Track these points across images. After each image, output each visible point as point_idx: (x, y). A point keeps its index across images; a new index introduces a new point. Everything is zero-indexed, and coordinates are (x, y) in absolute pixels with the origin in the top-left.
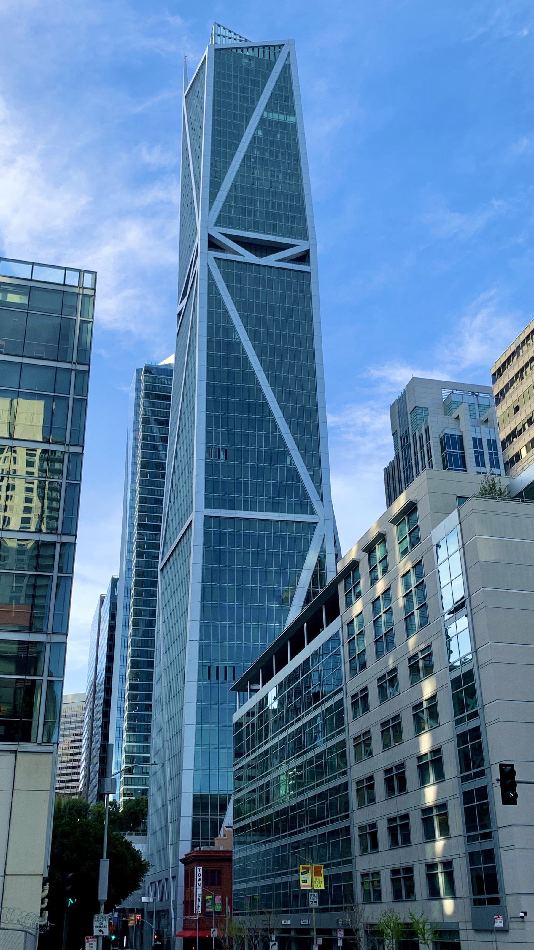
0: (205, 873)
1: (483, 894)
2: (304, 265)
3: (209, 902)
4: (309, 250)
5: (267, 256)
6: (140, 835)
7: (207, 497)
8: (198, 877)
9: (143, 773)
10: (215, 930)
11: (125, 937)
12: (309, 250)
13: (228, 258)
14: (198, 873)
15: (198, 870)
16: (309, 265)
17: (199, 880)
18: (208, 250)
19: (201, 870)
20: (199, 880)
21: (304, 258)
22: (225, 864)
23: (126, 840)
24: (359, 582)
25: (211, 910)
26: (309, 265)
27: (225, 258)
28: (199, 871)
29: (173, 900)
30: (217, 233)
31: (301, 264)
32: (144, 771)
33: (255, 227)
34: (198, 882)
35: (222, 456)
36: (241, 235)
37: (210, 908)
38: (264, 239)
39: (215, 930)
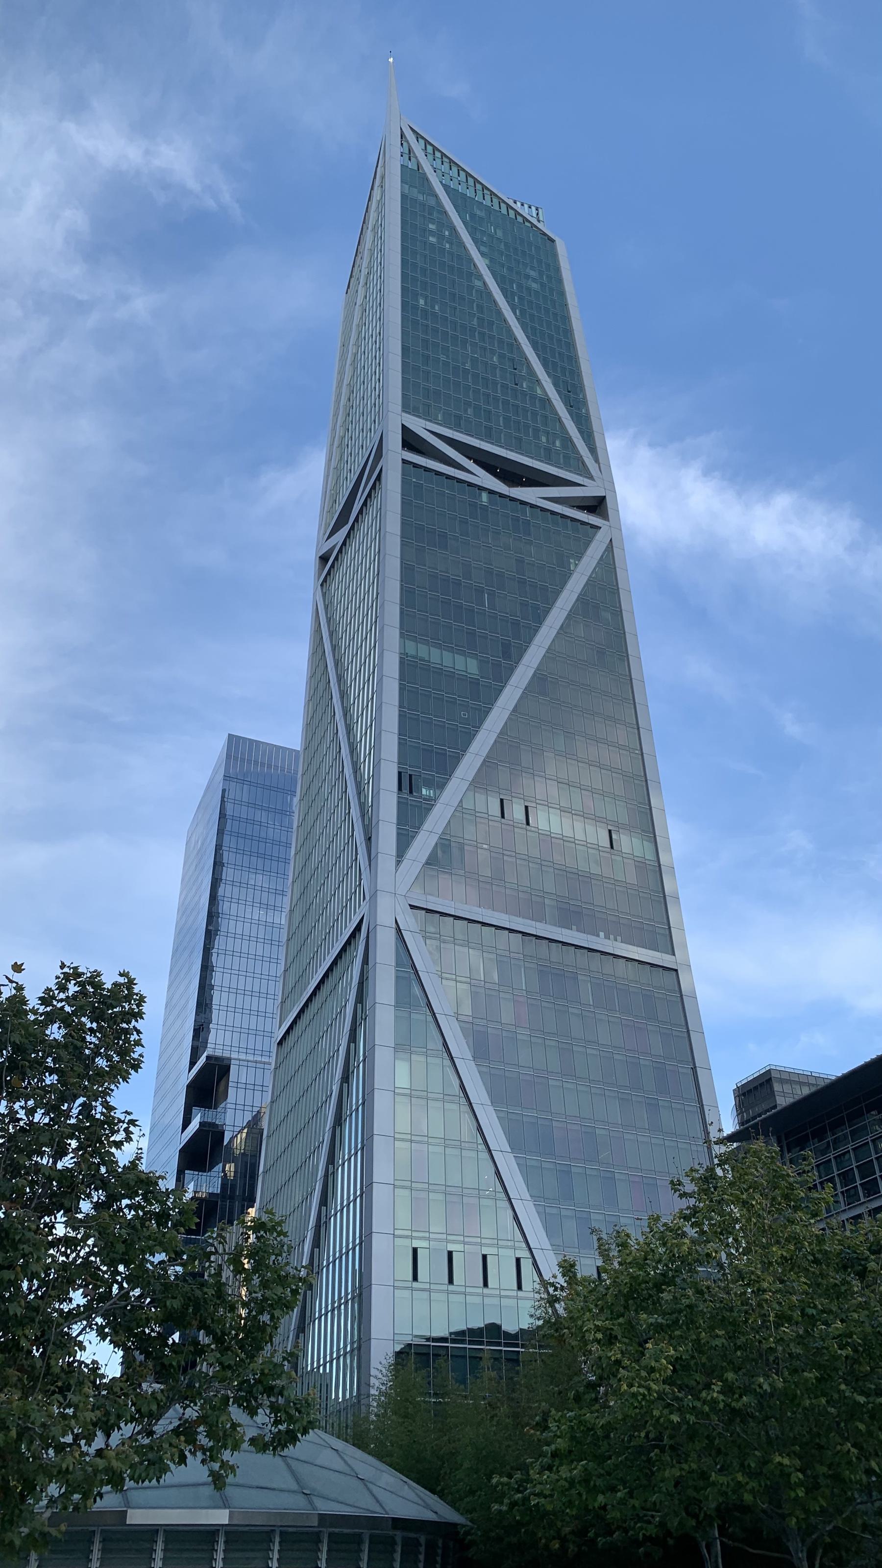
30: (418, 426)
33: (488, 436)
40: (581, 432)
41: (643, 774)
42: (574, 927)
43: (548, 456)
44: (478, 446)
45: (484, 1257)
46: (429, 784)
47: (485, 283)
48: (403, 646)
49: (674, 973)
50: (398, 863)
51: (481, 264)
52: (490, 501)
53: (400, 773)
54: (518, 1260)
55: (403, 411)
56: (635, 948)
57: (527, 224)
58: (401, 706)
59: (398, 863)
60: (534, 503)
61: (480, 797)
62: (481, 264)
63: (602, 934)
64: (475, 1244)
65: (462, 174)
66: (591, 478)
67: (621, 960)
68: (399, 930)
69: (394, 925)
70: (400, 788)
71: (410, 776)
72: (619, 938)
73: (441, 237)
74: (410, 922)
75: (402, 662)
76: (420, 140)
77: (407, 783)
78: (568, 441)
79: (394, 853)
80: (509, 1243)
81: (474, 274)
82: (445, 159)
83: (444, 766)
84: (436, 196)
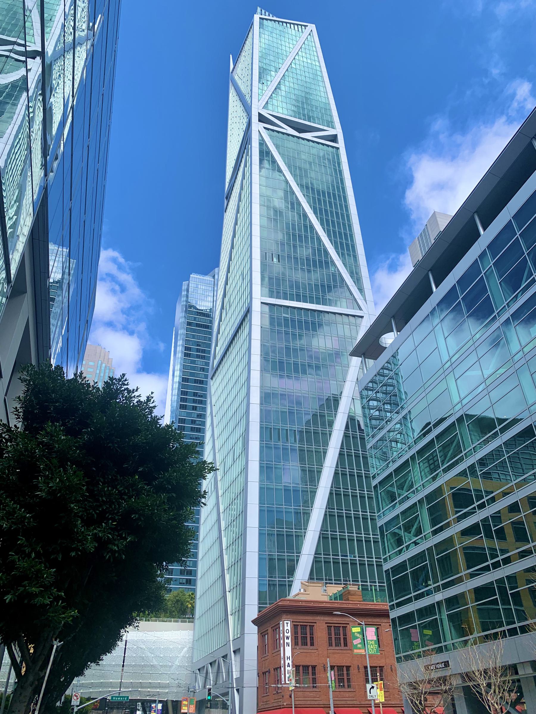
0: (295, 627)
3: (357, 638)
6: (186, 622)
8: (286, 634)
9: (180, 583)
10: (373, 687)
14: (286, 628)
15: (285, 625)
17: (288, 638)
19: (289, 625)
20: (288, 638)
22: (318, 618)
24: (358, 421)
25: (362, 652)
28: (286, 626)
29: (236, 679)
32: (181, 582)
34: (286, 641)
35: (275, 260)
37: (360, 649)
39: (373, 687)
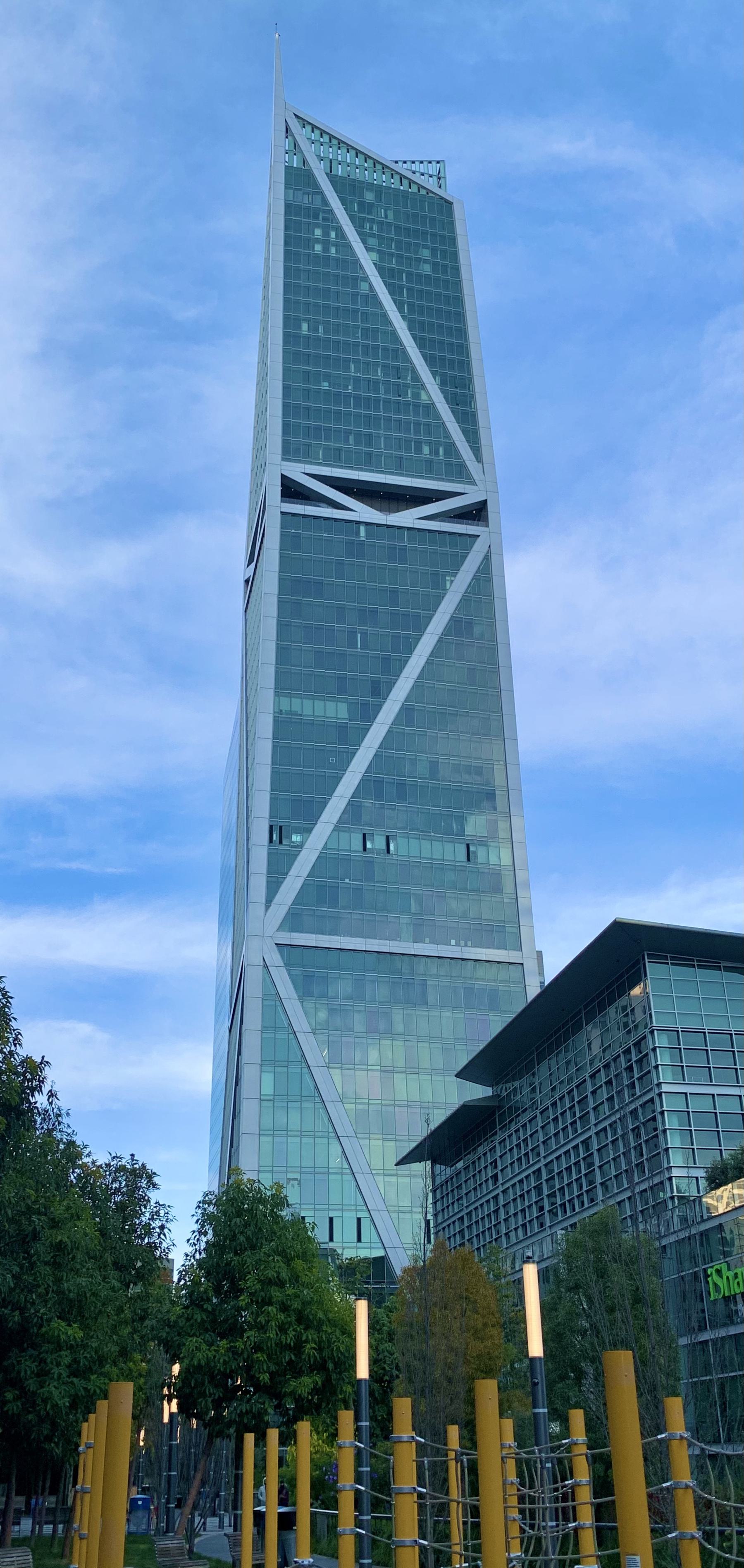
1: (525, 1504)
2: (478, 525)
4: (486, 501)
5: (398, 511)
7: (270, 879)
11: (536, 1348)
12: (486, 501)
13: (307, 513)
16: (487, 526)
18: (282, 501)
21: (477, 513)
23: (405, 1271)
26: (487, 526)
27: (302, 513)
30: (298, 472)
31: (462, 524)
33: (369, 462)
36: (383, 481)
38: (410, 485)
40: (465, 432)
41: (505, 784)
42: (427, 940)
43: (429, 469)
44: (356, 478)
45: (331, 1219)
46: (298, 831)
47: (371, 287)
48: (276, 703)
49: (520, 966)
50: (267, 907)
51: (367, 261)
52: (368, 535)
53: (271, 827)
54: (359, 1220)
55: (283, 459)
56: (483, 950)
57: (430, 195)
58: (274, 763)
59: (267, 907)
60: (411, 526)
61: (344, 836)
62: (367, 261)
63: (453, 942)
64: (324, 1210)
65: (405, 182)
66: (473, 483)
67: (470, 963)
68: (266, 966)
69: (262, 963)
70: (271, 840)
71: (281, 827)
72: (469, 943)
73: (326, 245)
74: (275, 958)
75: (276, 721)
76: (324, 135)
77: (277, 833)
78: (451, 449)
79: (264, 901)
80: (353, 1208)
81: (357, 276)
82: (342, 145)
83: (310, 813)
84: (322, 193)
